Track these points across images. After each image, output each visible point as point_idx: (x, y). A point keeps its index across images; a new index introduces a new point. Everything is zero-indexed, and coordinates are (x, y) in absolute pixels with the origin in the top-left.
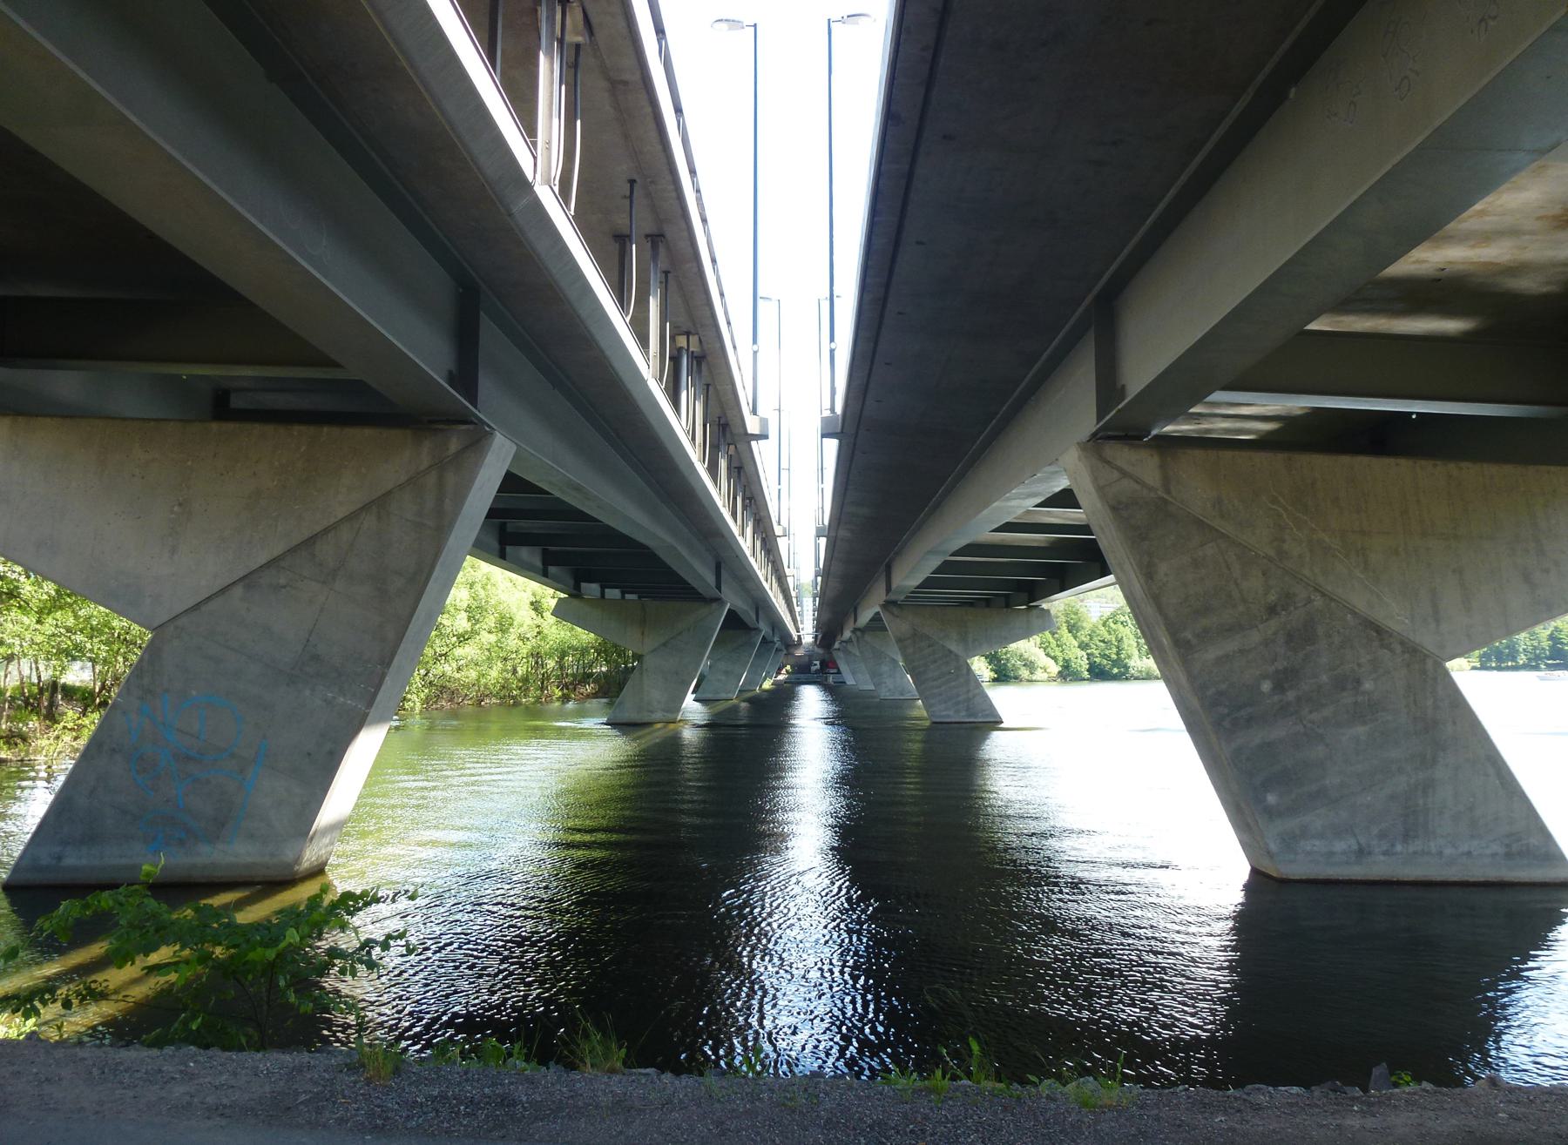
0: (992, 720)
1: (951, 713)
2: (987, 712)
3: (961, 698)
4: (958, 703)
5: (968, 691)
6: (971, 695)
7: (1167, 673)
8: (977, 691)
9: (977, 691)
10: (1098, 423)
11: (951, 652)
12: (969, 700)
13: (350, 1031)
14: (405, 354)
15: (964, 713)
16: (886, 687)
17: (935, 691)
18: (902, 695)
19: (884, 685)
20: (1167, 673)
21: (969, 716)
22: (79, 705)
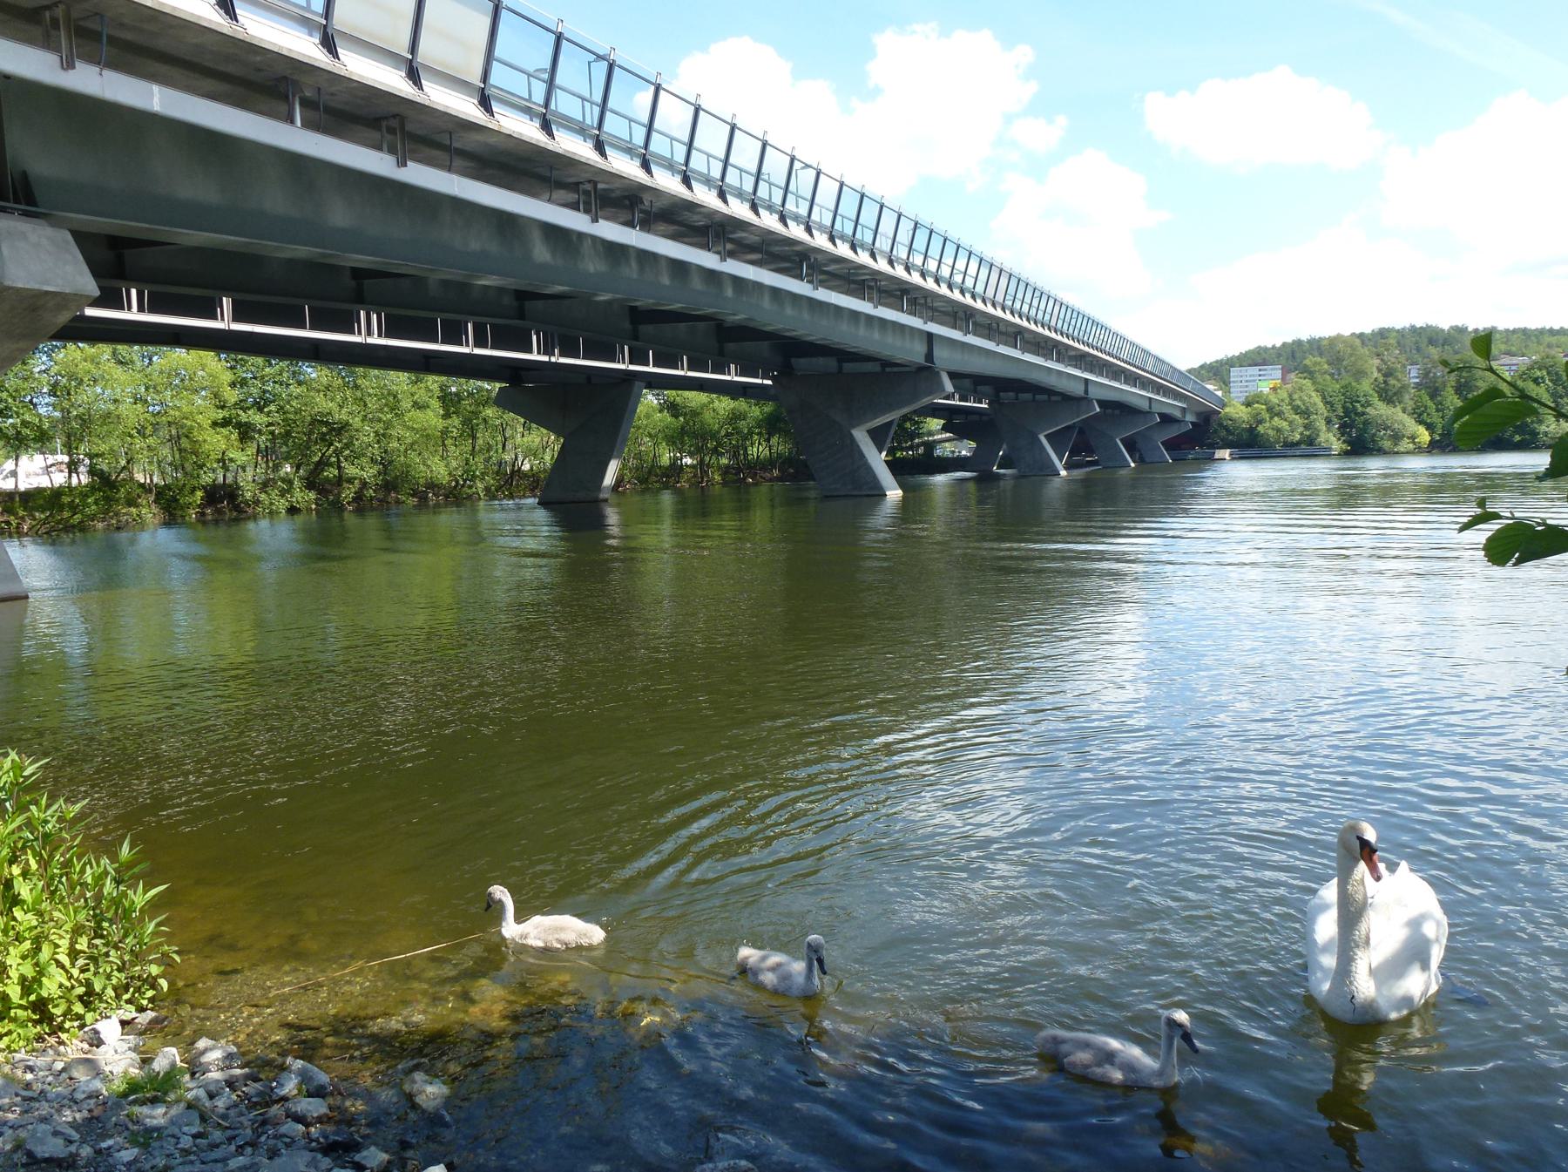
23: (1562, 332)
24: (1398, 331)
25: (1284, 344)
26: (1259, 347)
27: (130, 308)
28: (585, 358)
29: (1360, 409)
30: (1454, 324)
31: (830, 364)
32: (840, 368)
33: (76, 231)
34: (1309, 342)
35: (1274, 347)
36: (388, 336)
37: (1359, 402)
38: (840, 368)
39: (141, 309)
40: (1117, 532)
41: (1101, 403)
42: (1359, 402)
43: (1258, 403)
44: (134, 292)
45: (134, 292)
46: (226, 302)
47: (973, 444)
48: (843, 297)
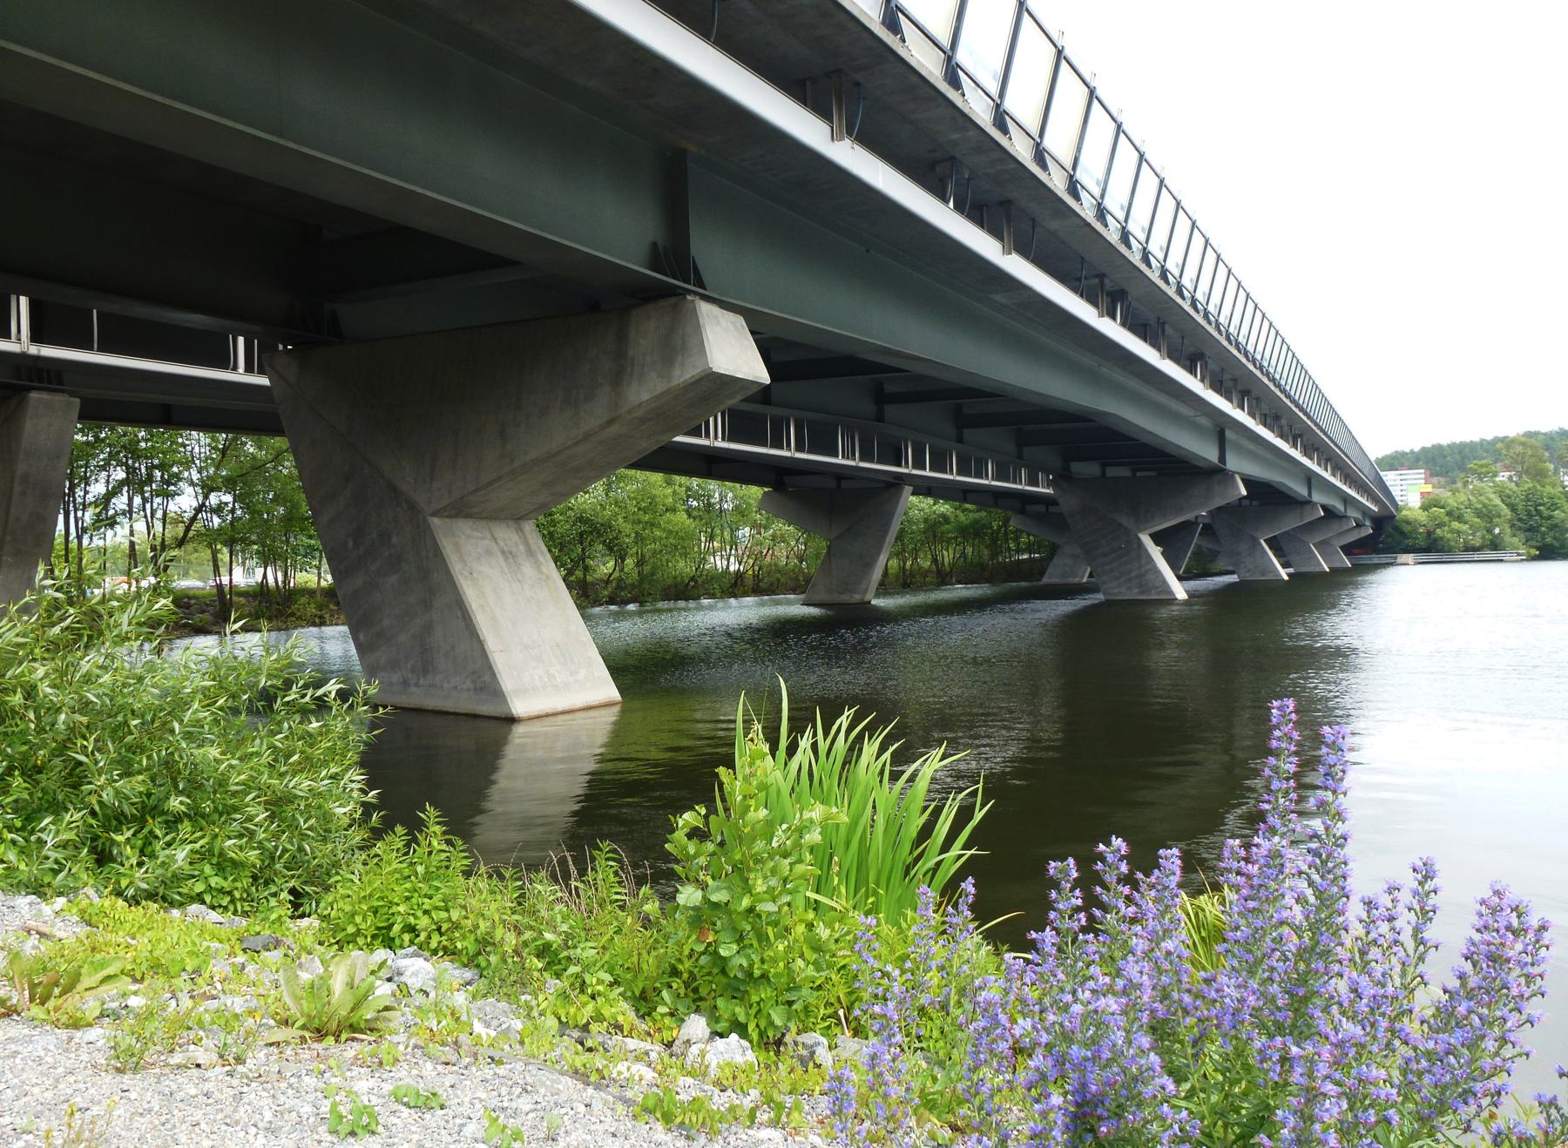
0: (1164, 597)
1: (1123, 590)
2: (1160, 589)
3: (1133, 574)
4: (1130, 580)
5: (1140, 566)
6: (1143, 570)
7: (446, 514)
8: (1149, 567)
9: (1149, 567)
10: (1196, 376)
11: (1121, 525)
12: (1141, 576)
13: (1122, 1075)
14: (541, 237)
15: (1136, 591)
16: (1245, 567)
17: (1107, 567)
18: (1263, 575)
19: (1242, 566)
20: (446, 514)
21: (1143, 593)
22: (200, 547)
23: (1565, 434)
24: (1545, 434)
25: (1423, 449)
26: (1397, 452)
27: (235, 368)
28: (879, 462)
29: (1546, 513)
30: (1399, 449)
31: (832, 484)
32: (1104, 474)
33: (1249, 480)
34: (1449, 446)
35: (1412, 452)
36: (731, 439)
37: (1543, 505)
38: (1104, 474)
39: (249, 369)
40: (1182, 758)
41: (1248, 482)
42: (1543, 505)
43: (1435, 506)
44: (241, 340)
45: (241, 340)
46: (22, 307)
47: (1114, 838)
48: (965, 839)
